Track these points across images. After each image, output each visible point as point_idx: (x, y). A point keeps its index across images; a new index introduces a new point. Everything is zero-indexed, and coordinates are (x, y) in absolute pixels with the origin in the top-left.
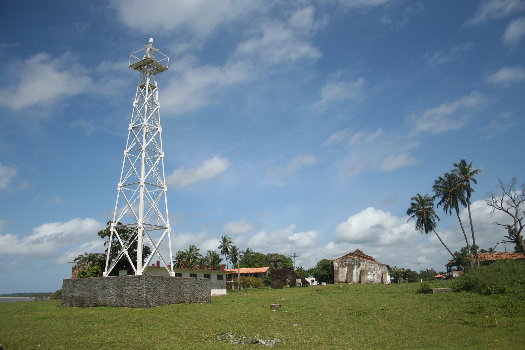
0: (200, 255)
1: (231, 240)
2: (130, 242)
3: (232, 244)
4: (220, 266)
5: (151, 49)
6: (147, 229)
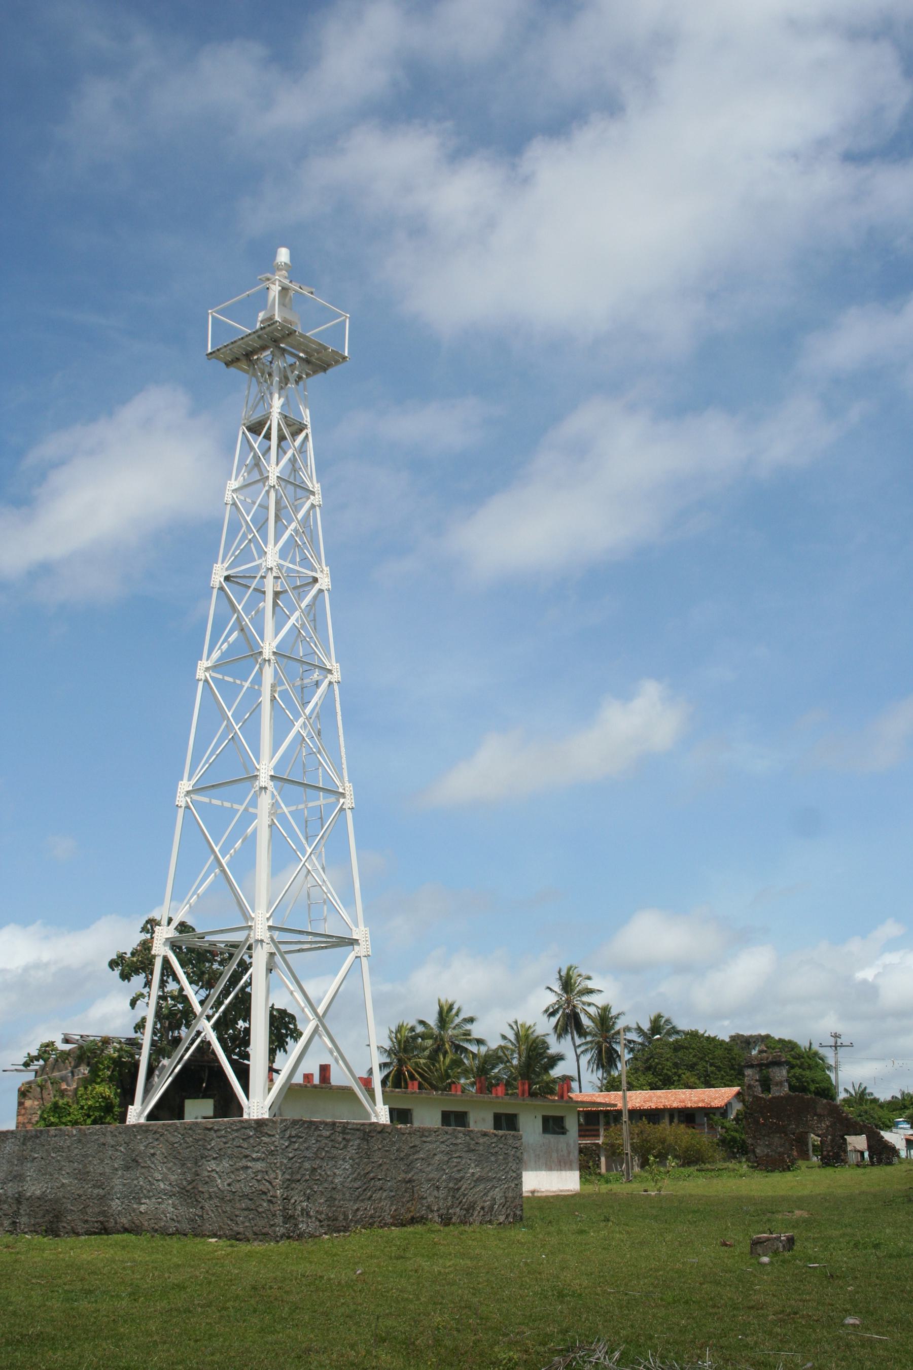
0: (480, 1042)
1: (590, 985)
2: (226, 992)
3: (598, 1000)
4: (554, 1081)
5: (284, 290)
6: (283, 948)
